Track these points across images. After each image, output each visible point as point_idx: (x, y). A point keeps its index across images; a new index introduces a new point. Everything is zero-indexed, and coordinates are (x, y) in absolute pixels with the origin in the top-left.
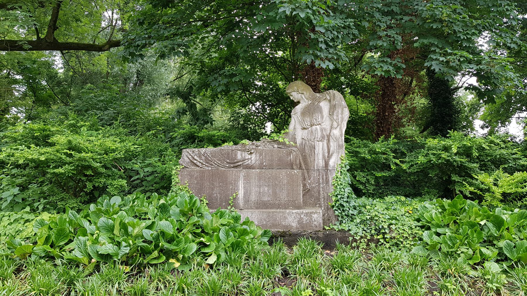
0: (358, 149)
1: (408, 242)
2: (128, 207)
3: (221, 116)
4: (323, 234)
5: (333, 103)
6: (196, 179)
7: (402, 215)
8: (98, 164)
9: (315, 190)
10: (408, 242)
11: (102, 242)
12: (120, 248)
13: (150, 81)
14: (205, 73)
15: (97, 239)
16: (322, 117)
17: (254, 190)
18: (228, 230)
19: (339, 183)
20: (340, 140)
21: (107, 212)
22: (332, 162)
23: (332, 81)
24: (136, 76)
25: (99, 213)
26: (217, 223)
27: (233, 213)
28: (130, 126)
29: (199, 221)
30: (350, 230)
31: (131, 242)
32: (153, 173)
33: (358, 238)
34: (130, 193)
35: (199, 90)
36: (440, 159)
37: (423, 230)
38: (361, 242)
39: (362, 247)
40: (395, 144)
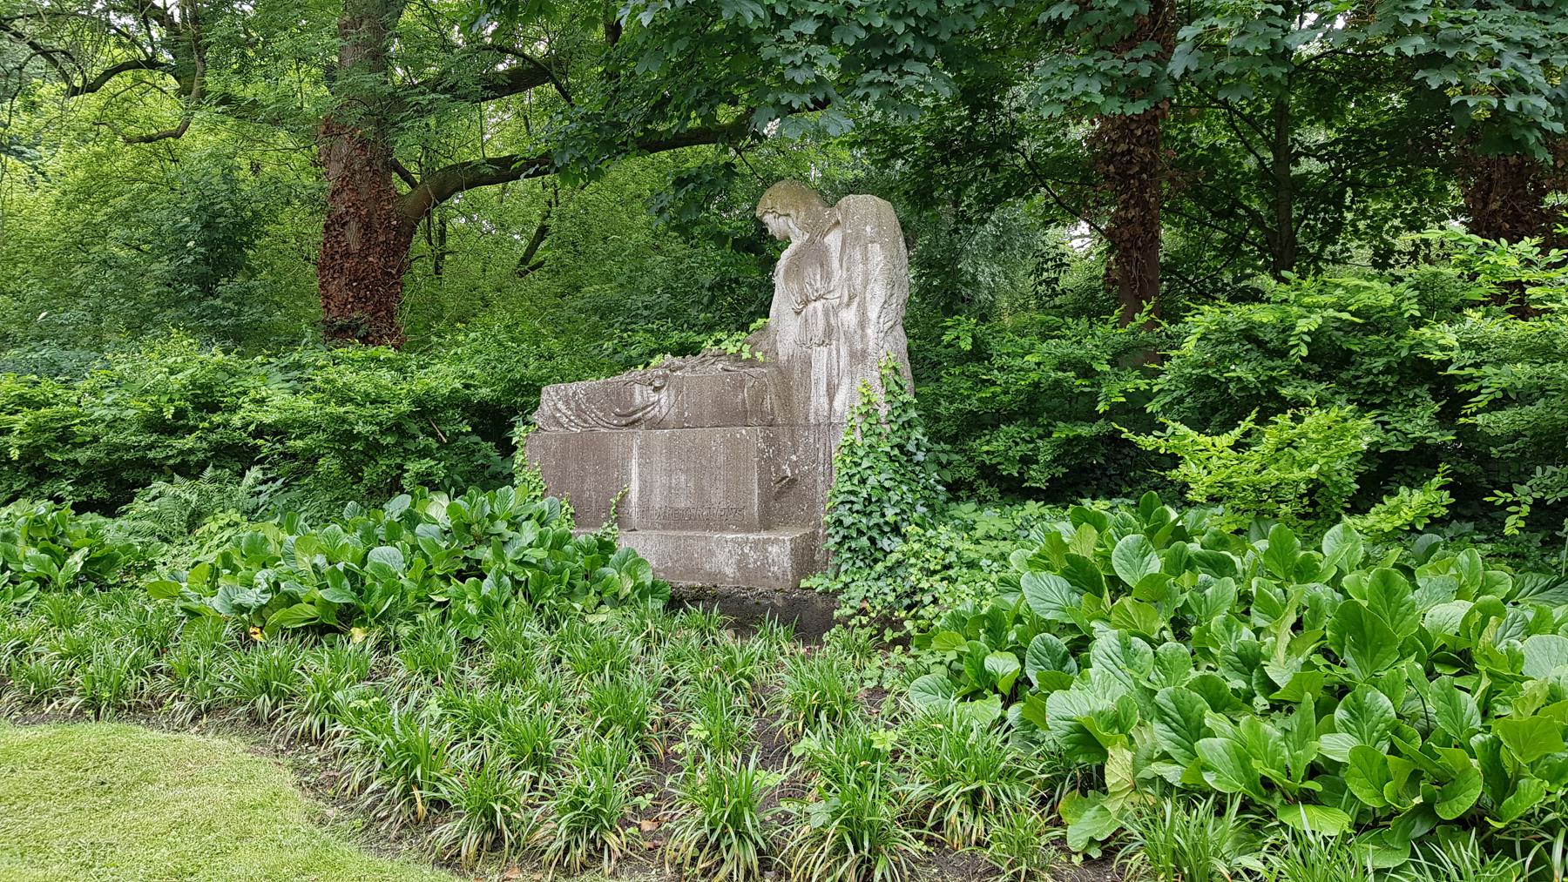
16: (827, 277)
17: (660, 480)
20: (857, 337)
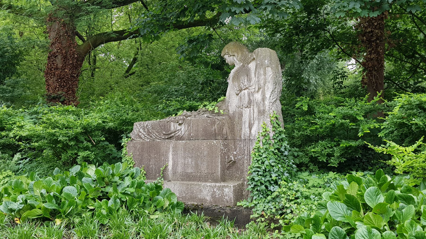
17: (181, 161)
20: (261, 105)
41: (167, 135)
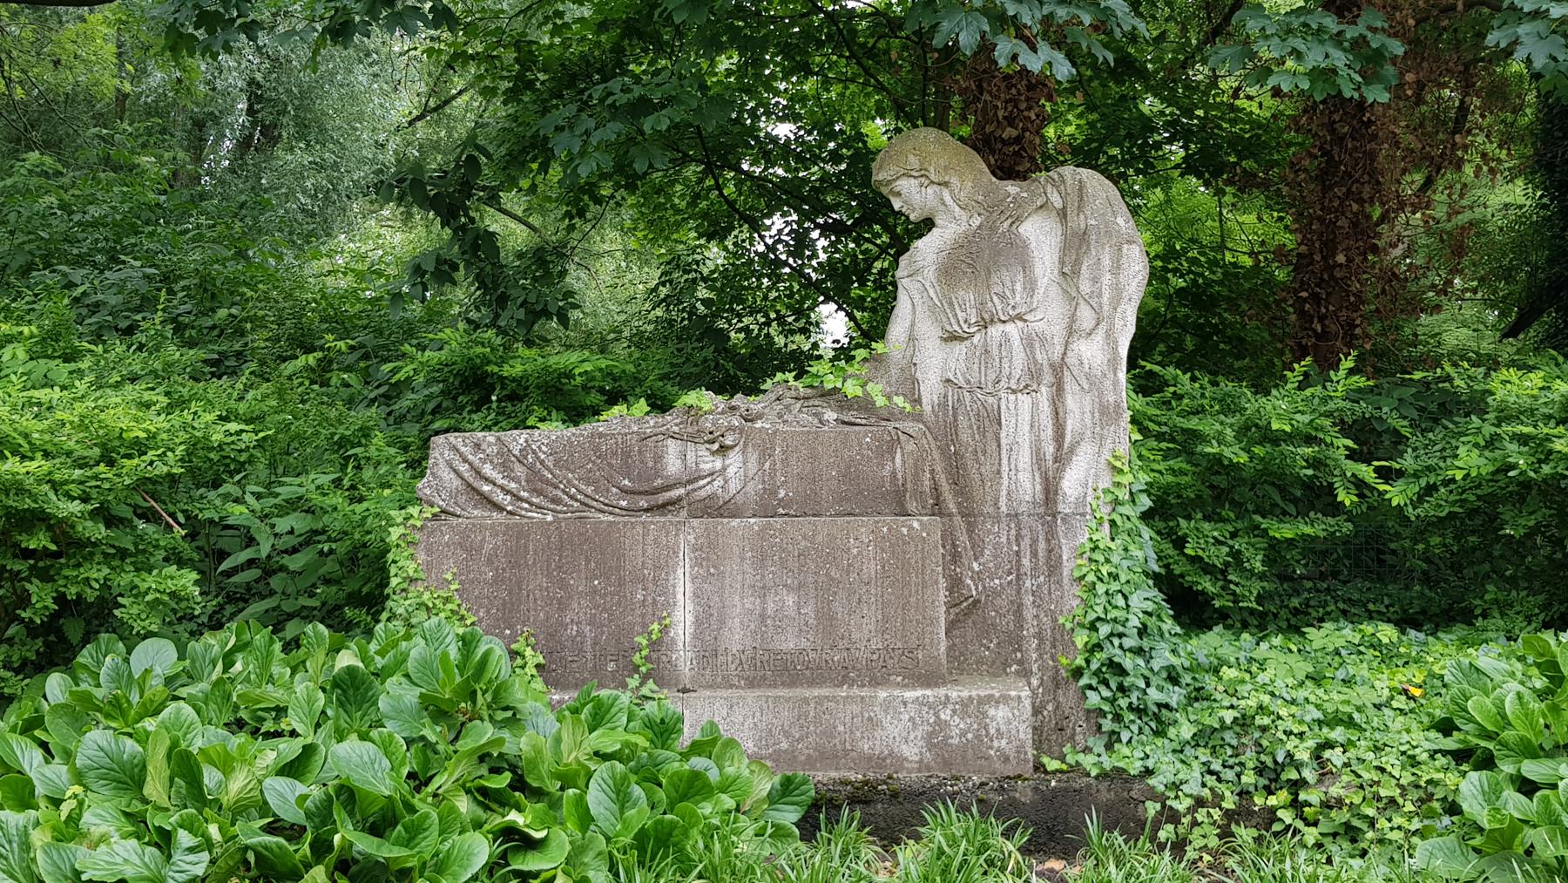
0: (1193, 423)
1: (1398, 820)
2: (204, 686)
3: (615, 277)
4: (1036, 789)
5: (1077, 222)
6: (490, 562)
7: (1378, 707)
8: (76, 507)
9: (1002, 602)
10: (1398, 820)
11: (96, 832)
12: (170, 856)
13: (309, 128)
14: (535, 91)
15: (73, 819)
18: (624, 778)
19: (1105, 570)
20: (1108, 383)
21: (116, 708)
22: (1071, 484)
23: (1103, 116)
24: (242, 106)
25: (81, 712)
26: (577, 747)
27: (650, 707)
28: (219, 331)
29: (501, 741)
30: (1149, 772)
31: (213, 830)
32: (311, 537)
33: (1182, 805)
34: (216, 625)
35: (513, 165)
36: (1546, 461)
37: (1465, 767)
38: (1195, 823)
39: (1199, 843)
40: (1355, 396)
41: (646, 493)
